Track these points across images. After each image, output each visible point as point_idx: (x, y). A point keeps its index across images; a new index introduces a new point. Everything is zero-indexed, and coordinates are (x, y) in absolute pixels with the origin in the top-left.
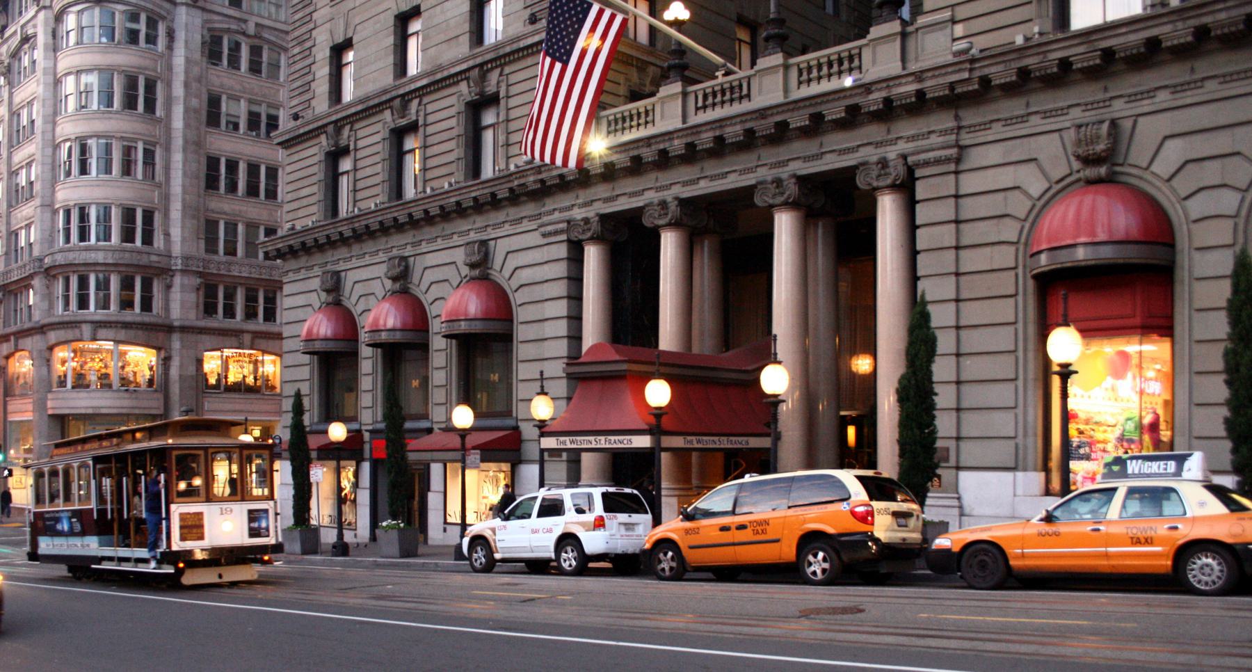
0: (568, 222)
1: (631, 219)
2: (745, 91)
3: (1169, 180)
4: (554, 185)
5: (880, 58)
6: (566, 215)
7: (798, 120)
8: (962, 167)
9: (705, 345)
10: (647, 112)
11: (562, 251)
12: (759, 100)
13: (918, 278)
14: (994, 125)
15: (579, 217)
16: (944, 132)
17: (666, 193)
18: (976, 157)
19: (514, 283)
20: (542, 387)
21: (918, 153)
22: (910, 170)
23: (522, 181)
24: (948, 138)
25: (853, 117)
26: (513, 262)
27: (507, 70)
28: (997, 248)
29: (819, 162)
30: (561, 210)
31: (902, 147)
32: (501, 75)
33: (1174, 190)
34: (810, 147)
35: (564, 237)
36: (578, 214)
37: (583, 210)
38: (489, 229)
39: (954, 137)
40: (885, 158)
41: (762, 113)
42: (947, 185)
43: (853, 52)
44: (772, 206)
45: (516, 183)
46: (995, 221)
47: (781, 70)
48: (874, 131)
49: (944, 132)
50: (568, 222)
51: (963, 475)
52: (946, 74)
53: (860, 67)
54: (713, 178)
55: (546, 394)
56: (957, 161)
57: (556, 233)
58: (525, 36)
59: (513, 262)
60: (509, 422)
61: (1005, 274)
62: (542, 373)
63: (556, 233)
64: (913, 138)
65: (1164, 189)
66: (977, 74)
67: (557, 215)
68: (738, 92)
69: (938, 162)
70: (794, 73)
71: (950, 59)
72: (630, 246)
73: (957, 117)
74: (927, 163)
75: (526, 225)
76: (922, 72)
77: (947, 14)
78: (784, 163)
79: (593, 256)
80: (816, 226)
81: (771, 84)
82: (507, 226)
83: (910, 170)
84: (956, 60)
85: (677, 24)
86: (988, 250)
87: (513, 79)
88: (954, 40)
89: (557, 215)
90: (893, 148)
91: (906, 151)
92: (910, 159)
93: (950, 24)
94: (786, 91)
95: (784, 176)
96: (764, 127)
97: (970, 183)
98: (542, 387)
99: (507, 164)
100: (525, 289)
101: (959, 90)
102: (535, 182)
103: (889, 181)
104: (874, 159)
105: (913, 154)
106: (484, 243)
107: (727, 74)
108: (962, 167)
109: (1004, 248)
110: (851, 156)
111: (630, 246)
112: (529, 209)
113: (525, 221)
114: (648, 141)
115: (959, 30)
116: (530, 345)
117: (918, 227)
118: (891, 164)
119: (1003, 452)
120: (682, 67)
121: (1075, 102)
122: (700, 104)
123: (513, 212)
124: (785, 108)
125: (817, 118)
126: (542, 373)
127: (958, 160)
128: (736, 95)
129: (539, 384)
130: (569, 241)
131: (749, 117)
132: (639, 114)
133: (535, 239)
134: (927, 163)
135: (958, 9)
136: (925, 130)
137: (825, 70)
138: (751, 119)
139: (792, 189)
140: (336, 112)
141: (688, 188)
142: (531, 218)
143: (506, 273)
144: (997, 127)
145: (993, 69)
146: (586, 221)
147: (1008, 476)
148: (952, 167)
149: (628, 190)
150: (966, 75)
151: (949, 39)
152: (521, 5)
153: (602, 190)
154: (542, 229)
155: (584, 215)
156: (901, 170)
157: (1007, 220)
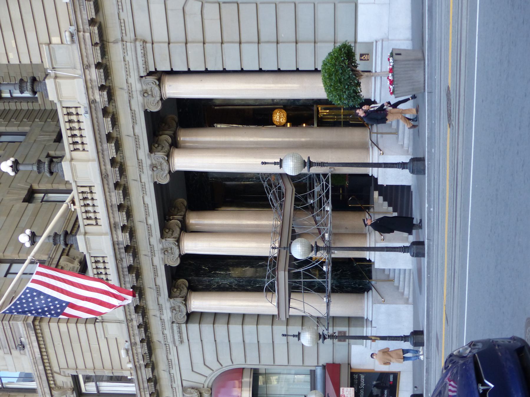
0: (173, 322)
1: (174, 275)
2: (87, 190)
3: (207, 377)
4: (143, 319)
5: (69, 91)
6: (168, 325)
7: (110, 150)
8: (149, 39)
9: (266, 220)
10: (69, 114)
11: (194, 327)
12: (82, 101)
13: (224, 69)
14: (122, 17)
15: (170, 314)
16: (125, 50)
17: (156, 249)
18: (143, 30)
19: (215, 366)
20: (294, 336)
21: (138, 68)
22: (150, 74)
23: (141, 357)
24: (129, 48)
25: (110, 113)
26: (199, 367)
27: (56, 369)
28: (205, 16)
29: (141, 138)
30: (164, 328)
31: (134, 79)
32: (60, 374)
33: (210, 375)
34: (128, 145)
35: (184, 326)
36: (167, 315)
37: (164, 311)
38: (174, 385)
39: (128, 44)
40: (162, 249)
41: (104, 177)
42: (161, 50)
43: (93, 261)
44: (170, 172)
45: (142, 362)
46: (187, 17)
47: (57, 80)
48: (121, 97)
49: (125, 50)
50: (173, 322)
51: (360, 39)
52: (97, 118)
53: (90, 187)
54: (147, 214)
55: (299, 333)
56: (146, 44)
57: (180, 332)
58: (33, 353)
59: (199, 367)
60: (319, 371)
61: (223, 11)
62: (283, 335)
63: (180, 332)
64: (128, 74)
65: (210, 378)
66: (87, 27)
67: (168, 332)
68: (87, 195)
69: (145, 55)
70: (75, 154)
71: (76, 47)
72: (194, 274)
73: (115, 42)
74: (146, 63)
75: (173, 356)
76: (116, 260)
77: (45, 48)
78: (140, 163)
79: (200, 303)
80: (185, 142)
81: (82, 167)
82: (172, 371)
83: (150, 74)
84: (77, 41)
85: (33, 238)
86: (206, 22)
87: (63, 364)
88: (62, 43)
89: (168, 332)
90: (133, 86)
91: (137, 77)
92: (142, 75)
93: (51, 45)
94: (101, 234)
95: (149, 162)
96: (113, 175)
97: (160, 34)
98: (294, 336)
99: (127, 370)
100: (220, 357)
101: (97, 40)
102: (142, 347)
103: (157, 88)
104: (140, 98)
105: (139, 72)
106: (184, 389)
107: (73, 202)
108: (149, 39)
109: (205, 11)
110: (137, 115)
111: (194, 274)
112: (160, 355)
113: (170, 357)
114: (118, 260)
115: (56, 40)
116: (262, 355)
117: (189, 69)
118: (145, 87)
119: (344, 10)
120: (66, 237)
121: (142, 198)
122: (93, 222)
123: (162, 366)
124: (101, 160)
125: (131, 269)
126: (283, 335)
127: (145, 42)
128: (103, 271)
129: (291, 339)
130: (187, 322)
131: (106, 186)
132: (70, 121)
133: (183, 350)
134: (146, 63)
135: (41, 41)
136: (123, 63)
137: (76, 125)
138: (108, 184)
139: (170, 242)
140: (32, 347)
141: (153, 232)
142: (168, 352)
143: (207, 372)
144: (123, 15)
145: (85, 17)
146: (173, 309)
147: (360, 8)
148: (149, 45)
149: (152, 275)
150: (87, 35)
151: (63, 45)
152: (8, 357)
153: (150, 296)
154: (177, 343)
155: (169, 311)
156: (151, 79)
157: (186, 9)
